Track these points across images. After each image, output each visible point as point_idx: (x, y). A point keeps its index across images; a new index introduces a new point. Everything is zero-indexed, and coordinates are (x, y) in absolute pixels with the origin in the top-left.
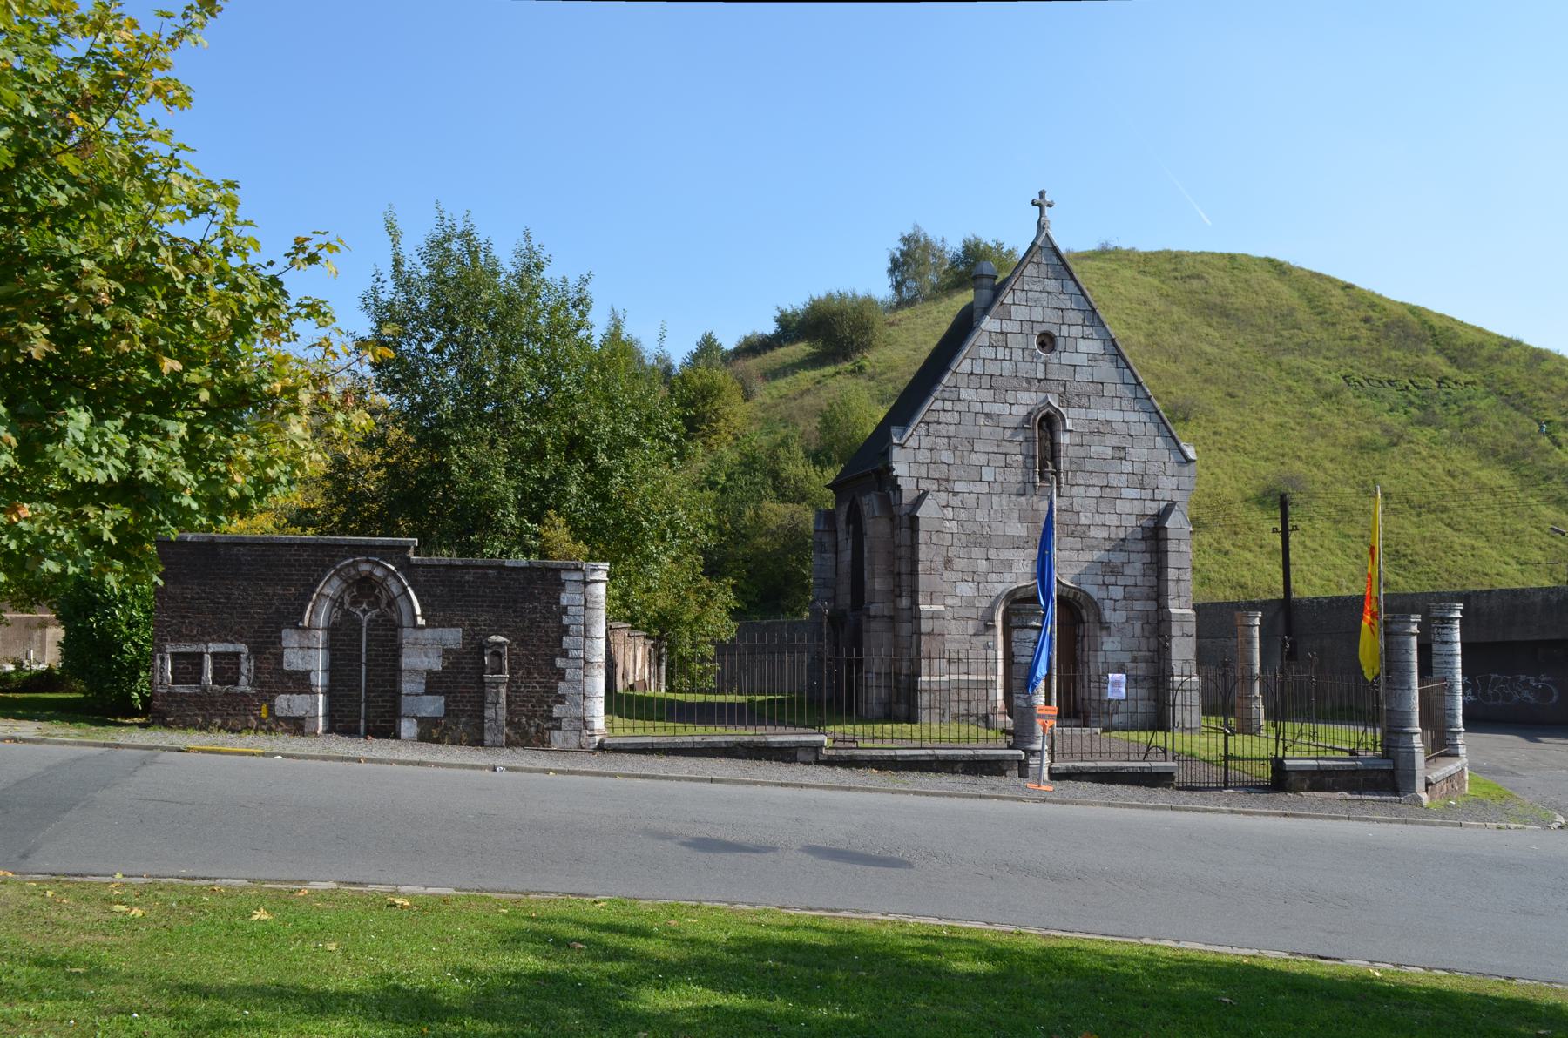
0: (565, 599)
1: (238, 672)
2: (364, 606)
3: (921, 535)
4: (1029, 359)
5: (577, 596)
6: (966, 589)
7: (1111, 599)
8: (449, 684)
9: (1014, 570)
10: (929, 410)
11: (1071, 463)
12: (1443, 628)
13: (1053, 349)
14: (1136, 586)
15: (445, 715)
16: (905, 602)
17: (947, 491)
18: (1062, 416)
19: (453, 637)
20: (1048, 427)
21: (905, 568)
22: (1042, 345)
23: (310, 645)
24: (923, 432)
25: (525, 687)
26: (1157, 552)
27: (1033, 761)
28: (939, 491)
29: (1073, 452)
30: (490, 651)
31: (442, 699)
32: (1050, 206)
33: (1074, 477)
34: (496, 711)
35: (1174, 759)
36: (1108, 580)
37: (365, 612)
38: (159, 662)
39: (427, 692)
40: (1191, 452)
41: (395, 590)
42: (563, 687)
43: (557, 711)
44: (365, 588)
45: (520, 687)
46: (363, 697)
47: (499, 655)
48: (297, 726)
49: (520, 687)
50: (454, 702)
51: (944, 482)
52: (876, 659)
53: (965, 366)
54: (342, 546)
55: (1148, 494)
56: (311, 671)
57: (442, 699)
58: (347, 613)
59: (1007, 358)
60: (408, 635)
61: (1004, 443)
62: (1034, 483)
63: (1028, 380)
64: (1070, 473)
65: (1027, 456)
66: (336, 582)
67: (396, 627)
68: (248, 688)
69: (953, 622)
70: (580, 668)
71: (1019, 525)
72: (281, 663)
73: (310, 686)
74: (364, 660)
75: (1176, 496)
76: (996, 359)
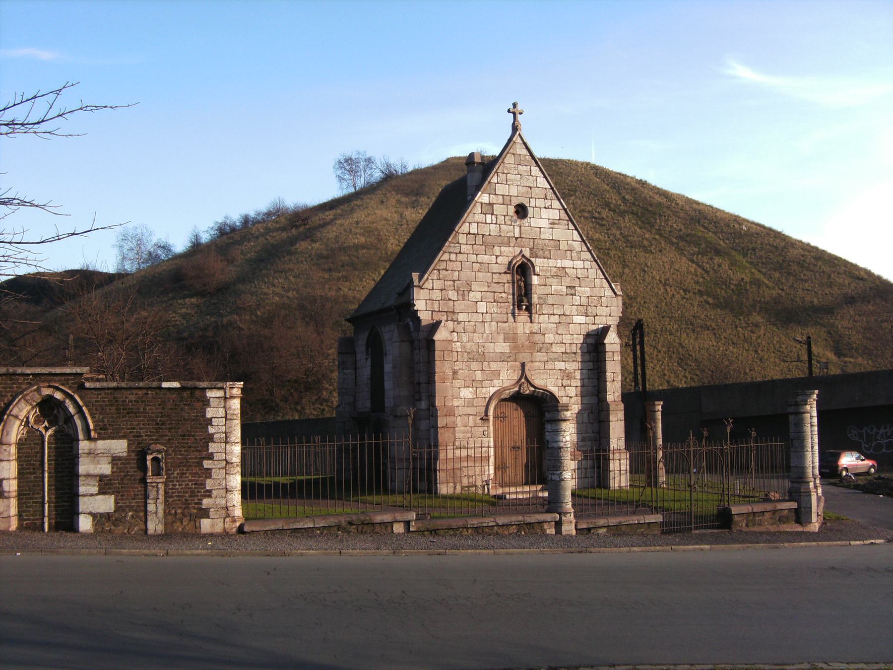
0: (210, 413)
2: (46, 423)
8: (118, 485)
9: (501, 378)
10: (439, 260)
11: (539, 298)
17: (452, 320)
18: (532, 264)
21: (423, 379)
22: (517, 212)
26: (597, 361)
31: (112, 498)
32: (521, 113)
36: (565, 382)
37: (46, 429)
45: (176, 485)
46: (46, 499)
49: (176, 485)
50: (122, 500)
53: (465, 228)
55: (590, 320)
57: (112, 498)
61: (493, 284)
64: (538, 305)
70: (223, 468)
76: (486, 223)
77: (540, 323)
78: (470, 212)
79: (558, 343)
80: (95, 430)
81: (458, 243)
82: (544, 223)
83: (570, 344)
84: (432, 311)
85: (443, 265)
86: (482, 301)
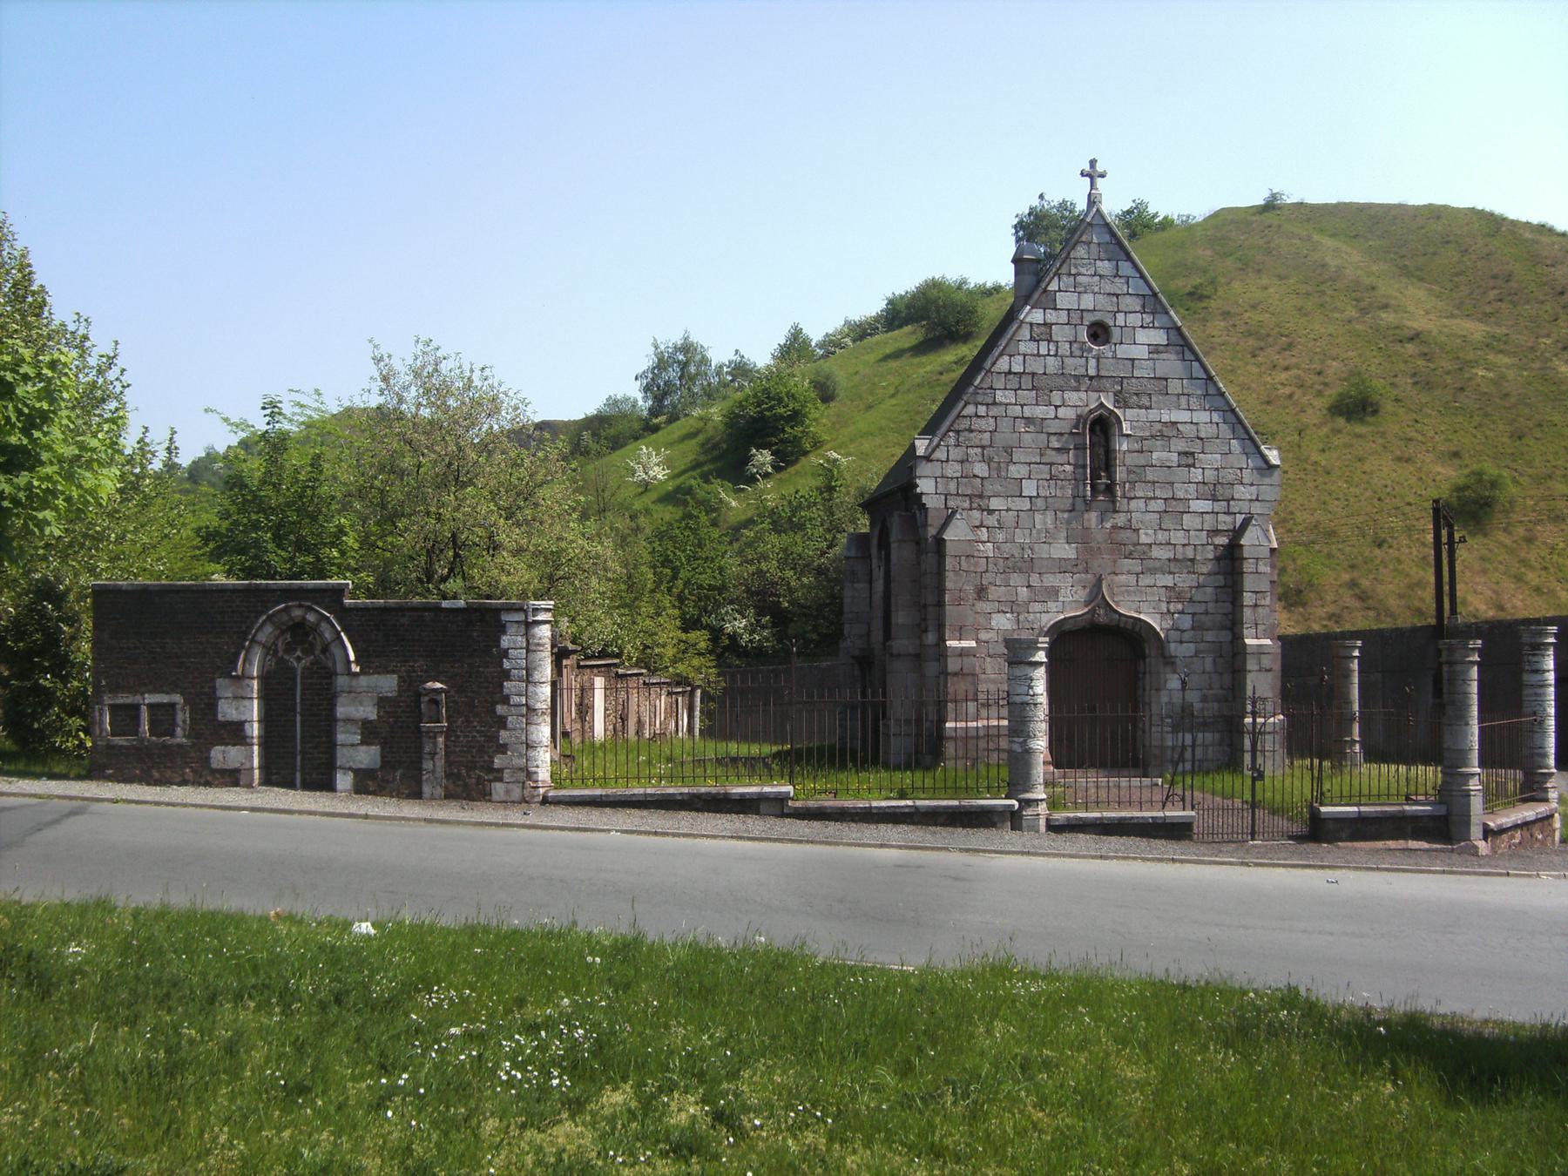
0: (505, 641)
1: (174, 724)
2: (299, 653)
3: (948, 560)
4: (1078, 353)
5: (519, 638)
6: (1003, 622)
7: (1177, 629)
9: (1061, 599)
10: (958, 416)
11: (1129, 472)
12: (1534, 655)
13: (1107, 341)
14: (1206, 613)
15: (381, 767)
16: (931, 638)
18: (1118, 418)
19: (388, 684)
20: (1101, 430)
23: (244, 695)
24: (952, 441)
25: (465, 736)
27: (1028, 812)
28: (971, 509)
29: (1131, 460)
30: (427, 698)
32: (1102, 176)
33: (1133, 488)
34: (434, 767)
35: (1193, 808)
37: (299, 659)
38: (97, 714)
39: (363, 742)
40: (1273, 456)
41: (328, 635)
42: (504, 736)
43: (498, 761)
44: (300, 633)
45: (459, 737)
46: (299, 748)
47: (436, 703)
48: (232, 778)
49: (459, 737)
51: (978, 500)
52: (899, 706)
54: (274, 591)
56: (246, 721)
58: (281, 661)
59: (1052, 353)
60: (341, 681)
61: (1049, 452)
62: (1084, 497)
63: (1077, 378)
64: (1127, 485)
65: (1076, 466)
66: (269, 629)
67: (330, 674)
68: (184, 740)
69: (988, 659)
70: (523, 716)
71: (1067, 546)
72: (215, 715)
73: (245, 737)
74: (298, 710)
75: (1257, 508)
76: (1038, 355)
77: (1131, 512)
78: (1011, 339)
79: (1161, 544)
80: (357, 662)
81: (991, 388)
82: (1140, 352)
83: (1184, 545)
84: (946, 495)
85: (964, 424)
86: (1030, 478)
